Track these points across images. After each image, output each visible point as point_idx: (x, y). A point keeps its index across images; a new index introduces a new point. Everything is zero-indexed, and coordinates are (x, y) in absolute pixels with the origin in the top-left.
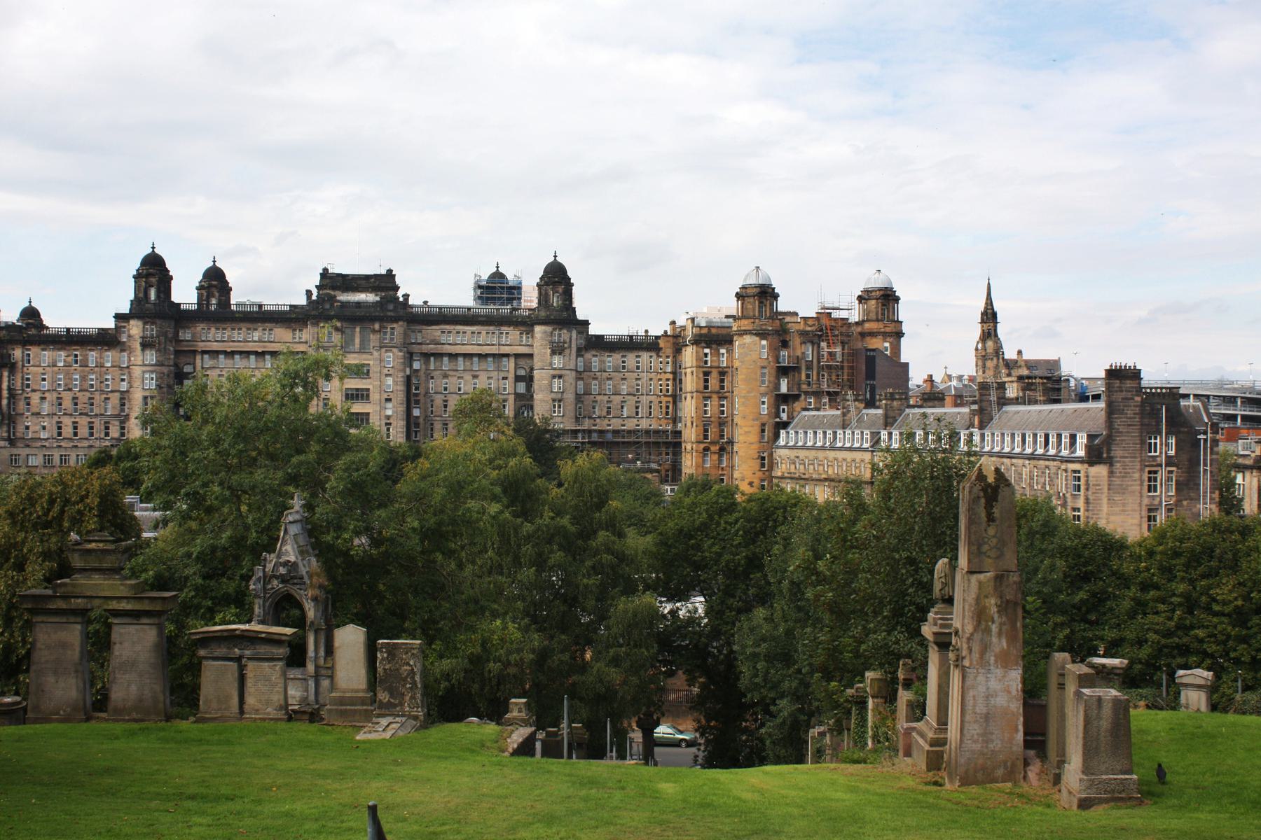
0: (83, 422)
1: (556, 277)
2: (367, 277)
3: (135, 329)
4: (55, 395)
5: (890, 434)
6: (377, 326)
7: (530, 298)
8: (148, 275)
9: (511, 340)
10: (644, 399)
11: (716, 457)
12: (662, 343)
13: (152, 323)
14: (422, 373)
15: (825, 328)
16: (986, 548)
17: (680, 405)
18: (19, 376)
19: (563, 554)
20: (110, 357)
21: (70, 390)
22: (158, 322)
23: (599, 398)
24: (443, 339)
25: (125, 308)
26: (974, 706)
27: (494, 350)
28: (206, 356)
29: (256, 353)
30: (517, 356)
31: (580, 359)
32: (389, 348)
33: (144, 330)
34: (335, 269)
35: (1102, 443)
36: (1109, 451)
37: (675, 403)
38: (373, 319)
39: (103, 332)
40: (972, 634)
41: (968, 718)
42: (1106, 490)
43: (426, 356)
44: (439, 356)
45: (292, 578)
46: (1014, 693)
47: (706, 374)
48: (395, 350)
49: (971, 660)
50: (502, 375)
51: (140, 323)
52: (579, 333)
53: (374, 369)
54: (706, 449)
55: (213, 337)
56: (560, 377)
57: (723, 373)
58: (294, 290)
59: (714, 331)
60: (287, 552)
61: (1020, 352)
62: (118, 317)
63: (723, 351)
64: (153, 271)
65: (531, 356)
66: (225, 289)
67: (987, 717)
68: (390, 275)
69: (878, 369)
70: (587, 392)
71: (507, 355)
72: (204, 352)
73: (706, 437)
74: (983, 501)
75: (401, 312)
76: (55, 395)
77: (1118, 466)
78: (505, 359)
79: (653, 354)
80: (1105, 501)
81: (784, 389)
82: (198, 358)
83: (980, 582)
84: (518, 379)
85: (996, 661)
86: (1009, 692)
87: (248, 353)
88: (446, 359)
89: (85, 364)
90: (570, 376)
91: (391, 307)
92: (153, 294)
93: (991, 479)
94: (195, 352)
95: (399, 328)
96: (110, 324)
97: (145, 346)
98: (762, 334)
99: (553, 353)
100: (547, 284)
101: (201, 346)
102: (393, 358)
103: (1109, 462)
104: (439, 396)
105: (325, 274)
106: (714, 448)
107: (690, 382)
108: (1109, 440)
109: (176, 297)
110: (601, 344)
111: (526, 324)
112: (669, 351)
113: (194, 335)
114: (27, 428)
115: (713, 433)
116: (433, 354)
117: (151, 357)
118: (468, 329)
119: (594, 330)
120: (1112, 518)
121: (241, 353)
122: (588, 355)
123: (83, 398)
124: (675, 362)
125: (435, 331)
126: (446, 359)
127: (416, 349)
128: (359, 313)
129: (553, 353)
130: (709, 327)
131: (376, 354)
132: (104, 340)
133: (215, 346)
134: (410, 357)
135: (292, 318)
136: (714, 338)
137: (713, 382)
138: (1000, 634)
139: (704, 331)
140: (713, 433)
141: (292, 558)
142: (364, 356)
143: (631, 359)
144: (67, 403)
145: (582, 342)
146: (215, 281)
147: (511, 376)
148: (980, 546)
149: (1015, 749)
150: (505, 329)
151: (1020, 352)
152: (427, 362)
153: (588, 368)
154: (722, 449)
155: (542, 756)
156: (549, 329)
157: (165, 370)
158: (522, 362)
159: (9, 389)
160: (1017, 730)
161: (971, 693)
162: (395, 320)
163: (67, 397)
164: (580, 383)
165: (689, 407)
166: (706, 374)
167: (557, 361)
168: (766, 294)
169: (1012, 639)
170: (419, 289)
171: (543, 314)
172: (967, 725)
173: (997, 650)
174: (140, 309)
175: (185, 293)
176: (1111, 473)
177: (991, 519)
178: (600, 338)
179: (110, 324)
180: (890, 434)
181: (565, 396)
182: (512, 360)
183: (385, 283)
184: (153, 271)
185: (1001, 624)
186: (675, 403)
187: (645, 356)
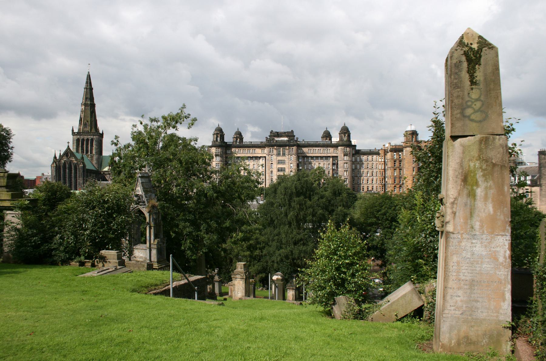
1: (345, 131)
2: (285, 133)
6: (287, 148)
7: (335, 139)
8: (217, 134)
9: (331, 152)
10: (375, 171)
11: (398, 189)
12: (380, 152)
14: (302, 163)
16: (469, 111)
17: (386, 172)
25: (210, 144)
26: (458, 272)
27: (325, 155)
30: (333, 157)
31: (353, 158)
35: (537, 178)
36: (540, 181)
37: (385, 172)
38: (286, 146)
40: (456, 199)
41: (451, 284)
42: (539, 196)
45: (140, 202)
46: (501, 259)
47: (395, 161)
49: (455, 225)
52: (353, 149)
53: (287, 161)
54: (395, 186)
55: (239, 153)
57: (400, 161)
60: (138, 190)
65: (337, 157)
66: (241, 139)
67: (472, 284)
68: (292, 131)
70: (356, 168)
71: (329, 157)
73: (395, 182)
74: (465, 65)
75: (295, 143)
77: (544, 187)
80: (538, 200)
83: (463, 146)
84: (333, 164)
85: (482, 226)
86: (496, 259)
91: (292, 141)
93: (475, 46)
95: (295, 148)
99: (344, 155)
100: (342, 133)
102: (294, 158)
103: (540, 185)
105: (271, 132)
106: (398, 186)
107: (390, 164)
108: (540, 178)
109: (226, 140)
111: (336, 146)
112: (383, 155)
115: (397, 181)
117: (219, 159)
118: (317, 148)
119: (357, 148)
120: (542, 207)
122: (356, 156)
124: (385, 158)
125: (305, 150)
127: (300, 155)
129: (344, 155)
134: (298, 157)
136: (397, 150)
137: (397, 164)
138: (486, 198)
139: (394, 147)
140: (397, 181)
141: (140, 193)
143: (370, 157)
145: (354, 152)
146: (239, 136)
147: (331, 163)
148: (463, 110)
149: (502, 318)
150: (329, 148)
152: (304, 159)
153: (356, 160)
154: (400, 186)
156: (343, 148)
158: (334, 159)
160: (504, 300)
161: (455, 259)
162: (293, 146)
164: (353, 165)
165: (389, 173)
166: (395, 161)
167: (346, 158)
169: (498, 204)
170: (301, 136)
171: (341, 143)
172: (450, 291)
173: (483, 215)
175: (229, 138)
176: (541, 190)
177: (473, 82)
178: (359, 150)
184: (219, 133)
185: (486, 188)
186: (385, 172)
187: (375, 156)
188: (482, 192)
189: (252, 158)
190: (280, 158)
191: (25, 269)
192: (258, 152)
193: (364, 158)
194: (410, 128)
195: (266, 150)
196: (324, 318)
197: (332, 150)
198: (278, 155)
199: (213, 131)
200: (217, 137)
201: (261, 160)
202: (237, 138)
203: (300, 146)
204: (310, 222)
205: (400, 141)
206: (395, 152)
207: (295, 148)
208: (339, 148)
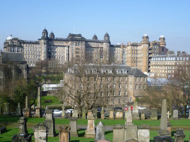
0: (33, 56)
1: (107, 35)
3: (42, 41)
4: (29, 52)
6: (81, 42)
10: (118, 55)
19: (49, 76)
20: (37, 46)
25: (40, 38)
47: (132, 50)
58: (65, 36)
59: (134, 44)
64: (45, 32)
66: (54, 36)
69: (164, 50)
76: (29, 52)
81: (150, 52)
88: (90, 48)
89: (33, 47)
95: (84, 42)
97: (44, 44)
98: (147, 44)
116: (88, 47)
123: (33, 52)
128: (78, 40)
130: (133, 43)
132: (37, 43)
144: (30, 53)
146: (52, 34)
155: (97, 113)
156: (106, 43)
162: (83, 41)
163: (30, 52)
166: (132, 50)
174: (43, 38)
178: (112, 45)
183: (80, 35)
184: (45, 32)
187: (119, 48)
188: (15, 72)
189: (61, 46)
190: (77, 47)
191: (6, 133)
192: (65, 44)
193: (116, 49)
194: (145, 35)
195: (70, 43)
196: (38, 99)
197: (100, 44)
198: (76, 45)
199: (42, 31)
200: (45, 34)
201: (66, 47)
202: (52, 36)
203: (87, 42)
204: (155, 75)
205: (139, 40)
206: (133, 46)
207: (84, 42)
208: (104, 43)
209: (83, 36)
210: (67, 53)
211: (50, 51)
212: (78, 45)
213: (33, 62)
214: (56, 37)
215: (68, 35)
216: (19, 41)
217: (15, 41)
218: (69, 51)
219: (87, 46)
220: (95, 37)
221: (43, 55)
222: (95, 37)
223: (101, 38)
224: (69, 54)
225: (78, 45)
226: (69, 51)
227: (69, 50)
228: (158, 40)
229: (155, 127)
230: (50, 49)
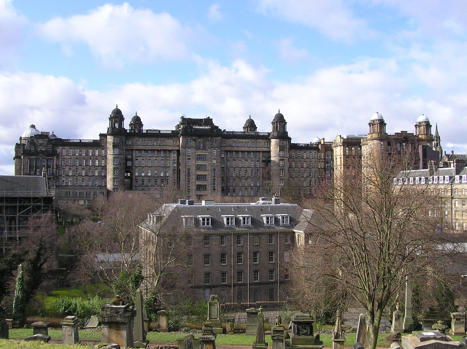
1: (280, 121)
4: (75, 167)
5: (461, 177)
6: (210, 139)
13: (117, 138)
15: (404, 138)
18: (60, 159)
21: (81, 165)
22: (120, 136)
23: (295, 169)
24: (234, 145)
27: (254, 149)
28: (137, 151)
29: (158, 150)
32: (214, 148)
33: (114, 140)
34: (187, 117)
38: (208, 136)
39: (95, 141)
43: (227, 151)
44: (231, 152)
48: (217, 149)
50: (257, 159)
51: (112, 137)
55: (140, 143)
56: (283, 160)
59: (349, 141)
61: (453, 152)
62: (101, 135)
63: (353, 148)
64: (117, 116)
71: (259, 152)
72: (137, 150)
78: (258, 153)
79: (316, 151)
82: (134, 152)
87: (153, 150)
90: (286, 160)
92: (117, 125)
94: (132, 150)
96: (98, 138)
101: (136, 148)
104: (232, 168)
110: (296, 147)
113: (132, 143)
114: (63, 181)
116: (229, 151)
121: (151, 150)
125: (230, 141)
126: (234, 153)
131: (209, 150)
133: (141, 147)
135: (174, 135)
142: (204, 151)
146: (137, 121)
151: (453, 152)
157: (122, 156)
159: (56, 165)
168: (382, 123)
179: (98, 138)
180: (461, 177)
181: (285, 168)
182: (261, 154)
184: (117, 116)
187: (313, 152)
193: (212, 346)
209: (215, 123)
210: (174, 170)
211: (129, 164)
212: (202, 147)
213: (85, 193)
214: (145, 128)
215: (178, 121)
216: (50, 141)
217: (41, 141)
218: (179, 164)
219: (268, 154)
220: (251, 124)
221: (110, 177)
222: (251, 124)
223: (264, 127)
224: (179, 171)
225: (202, 147)
226: (179, 164)
227: (180, 161)
228: (411, 130)
229: (408, 294)
230: (131, 160)
